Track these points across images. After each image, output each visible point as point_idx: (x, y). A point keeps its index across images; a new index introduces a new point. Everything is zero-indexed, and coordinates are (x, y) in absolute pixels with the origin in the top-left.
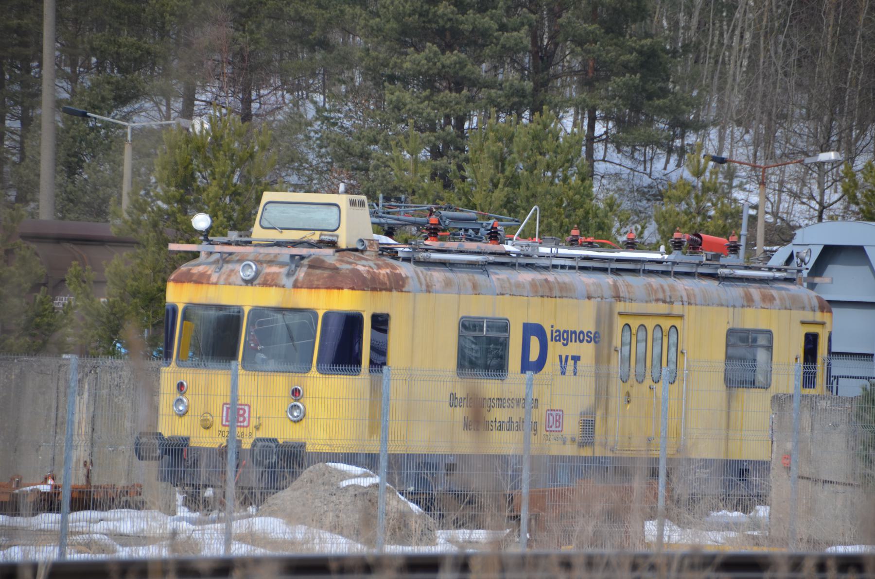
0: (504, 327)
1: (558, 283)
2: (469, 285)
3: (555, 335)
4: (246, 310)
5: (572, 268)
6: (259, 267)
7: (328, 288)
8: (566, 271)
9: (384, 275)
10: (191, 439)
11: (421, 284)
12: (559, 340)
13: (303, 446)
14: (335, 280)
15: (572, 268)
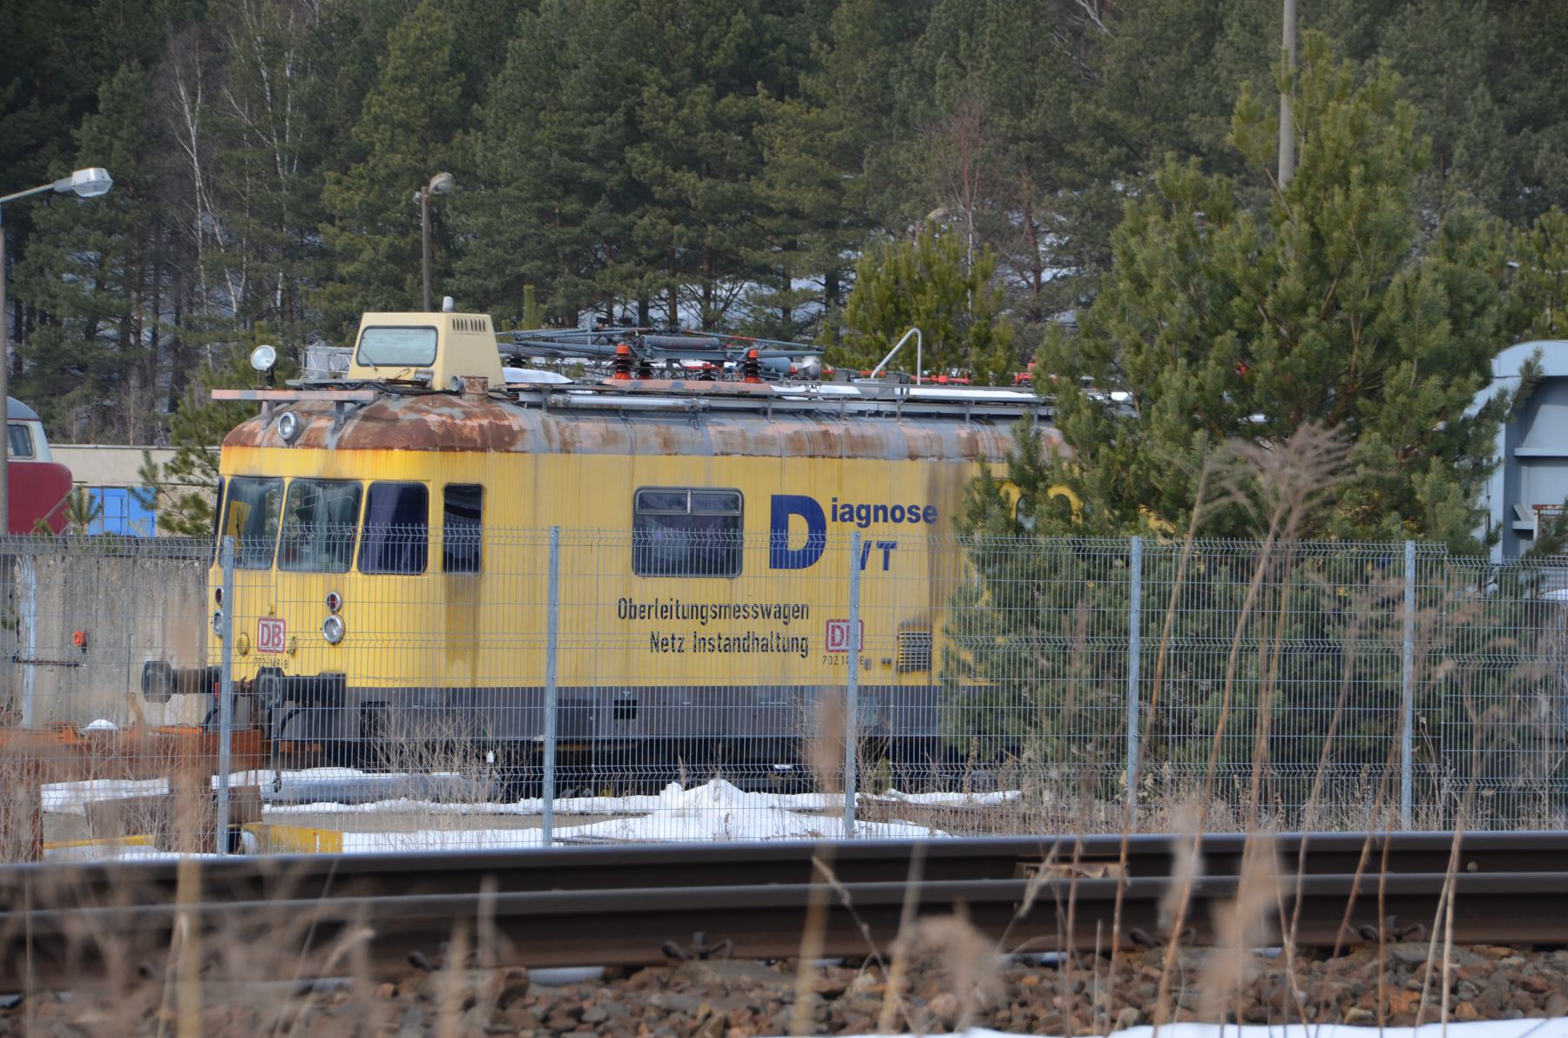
0: (734, 500)
1: (850, 436)
2: (655, 441)
3: (840, 511)
4: (287, 482)
5: (892, 415)
6: (303, 420)
7: (375, 448)
8: (882, 419)
9: (473, 428)
10: (350, 675)
11: (550, 440)
12: (851, 519)
13: (340, 679)
14: (386, 437)
15: (892, 415)
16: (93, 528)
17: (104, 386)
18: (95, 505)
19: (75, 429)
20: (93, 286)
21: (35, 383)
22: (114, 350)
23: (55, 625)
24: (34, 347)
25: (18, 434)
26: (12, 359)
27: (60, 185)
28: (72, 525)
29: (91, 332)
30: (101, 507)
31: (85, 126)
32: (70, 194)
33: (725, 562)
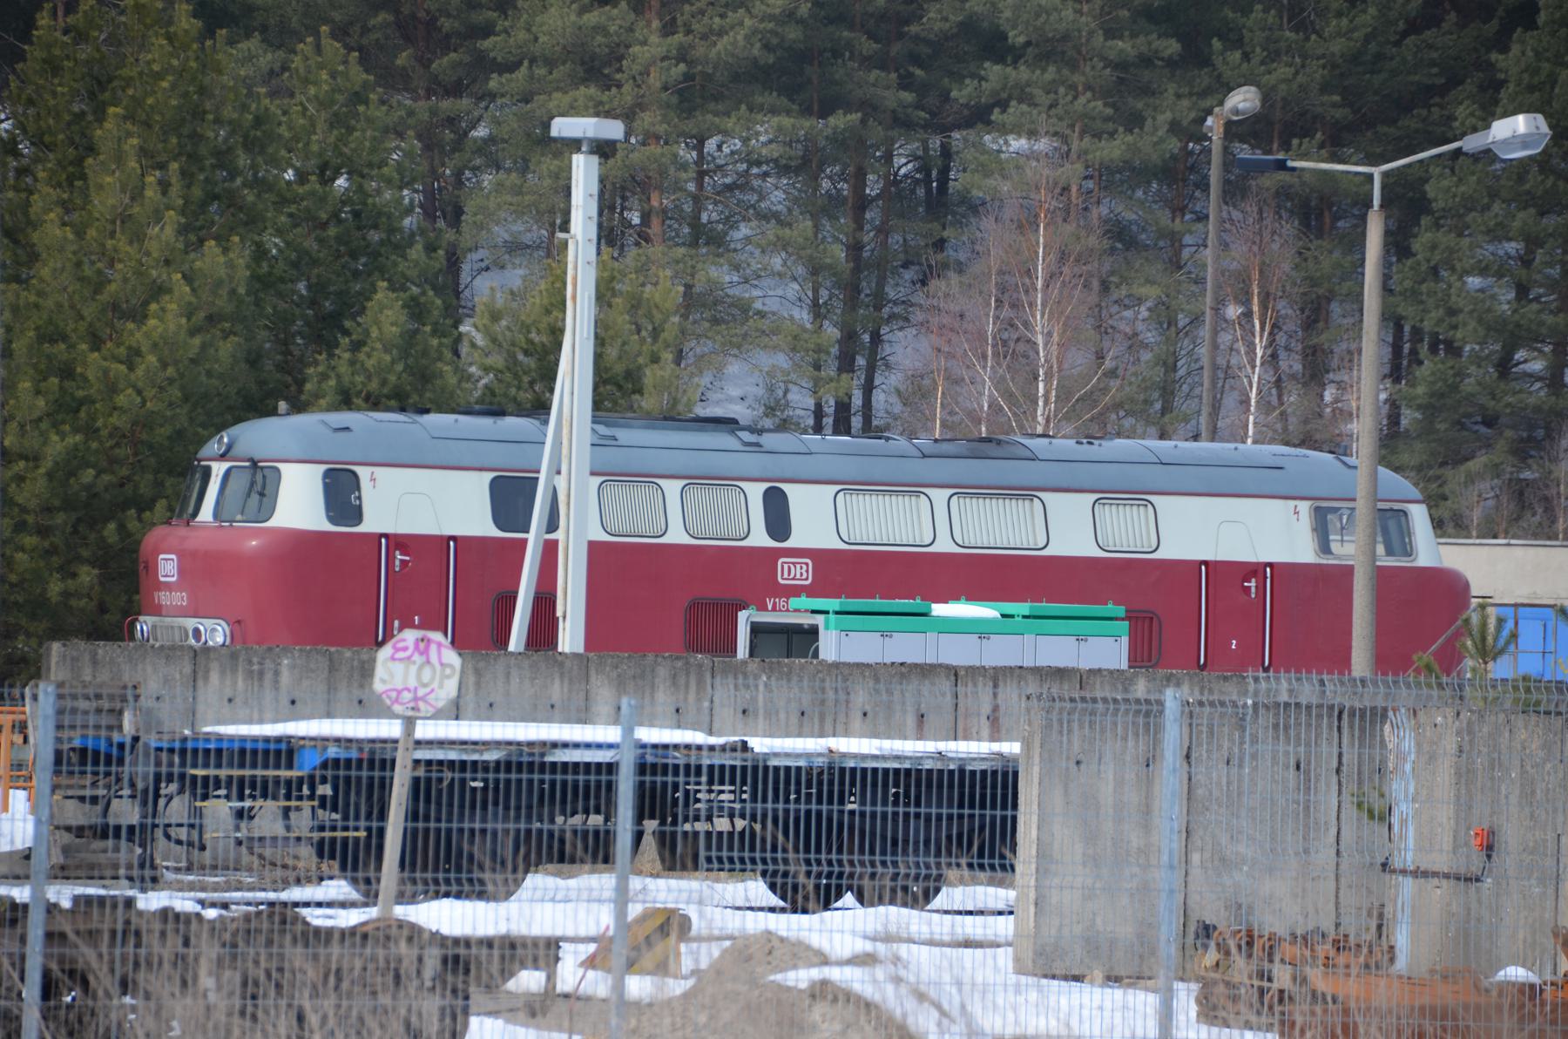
16: (1501, 669)
17: (1523, 451)
18: (1505, 633)
19: (1476, 516)
20: (1512, 295)
21: (1418, 446)
22: (1538, 393)
23: (1445, 814)
24: (1420, 390)
25: (1392, 525)
26: (1385, 410)
27: (1471, 143)
28: (1469, 663)
29: (1504, 366)
30: (1514, 636)
31: (1515, 49)
32: (1487, 155)
33: (556, 542)
